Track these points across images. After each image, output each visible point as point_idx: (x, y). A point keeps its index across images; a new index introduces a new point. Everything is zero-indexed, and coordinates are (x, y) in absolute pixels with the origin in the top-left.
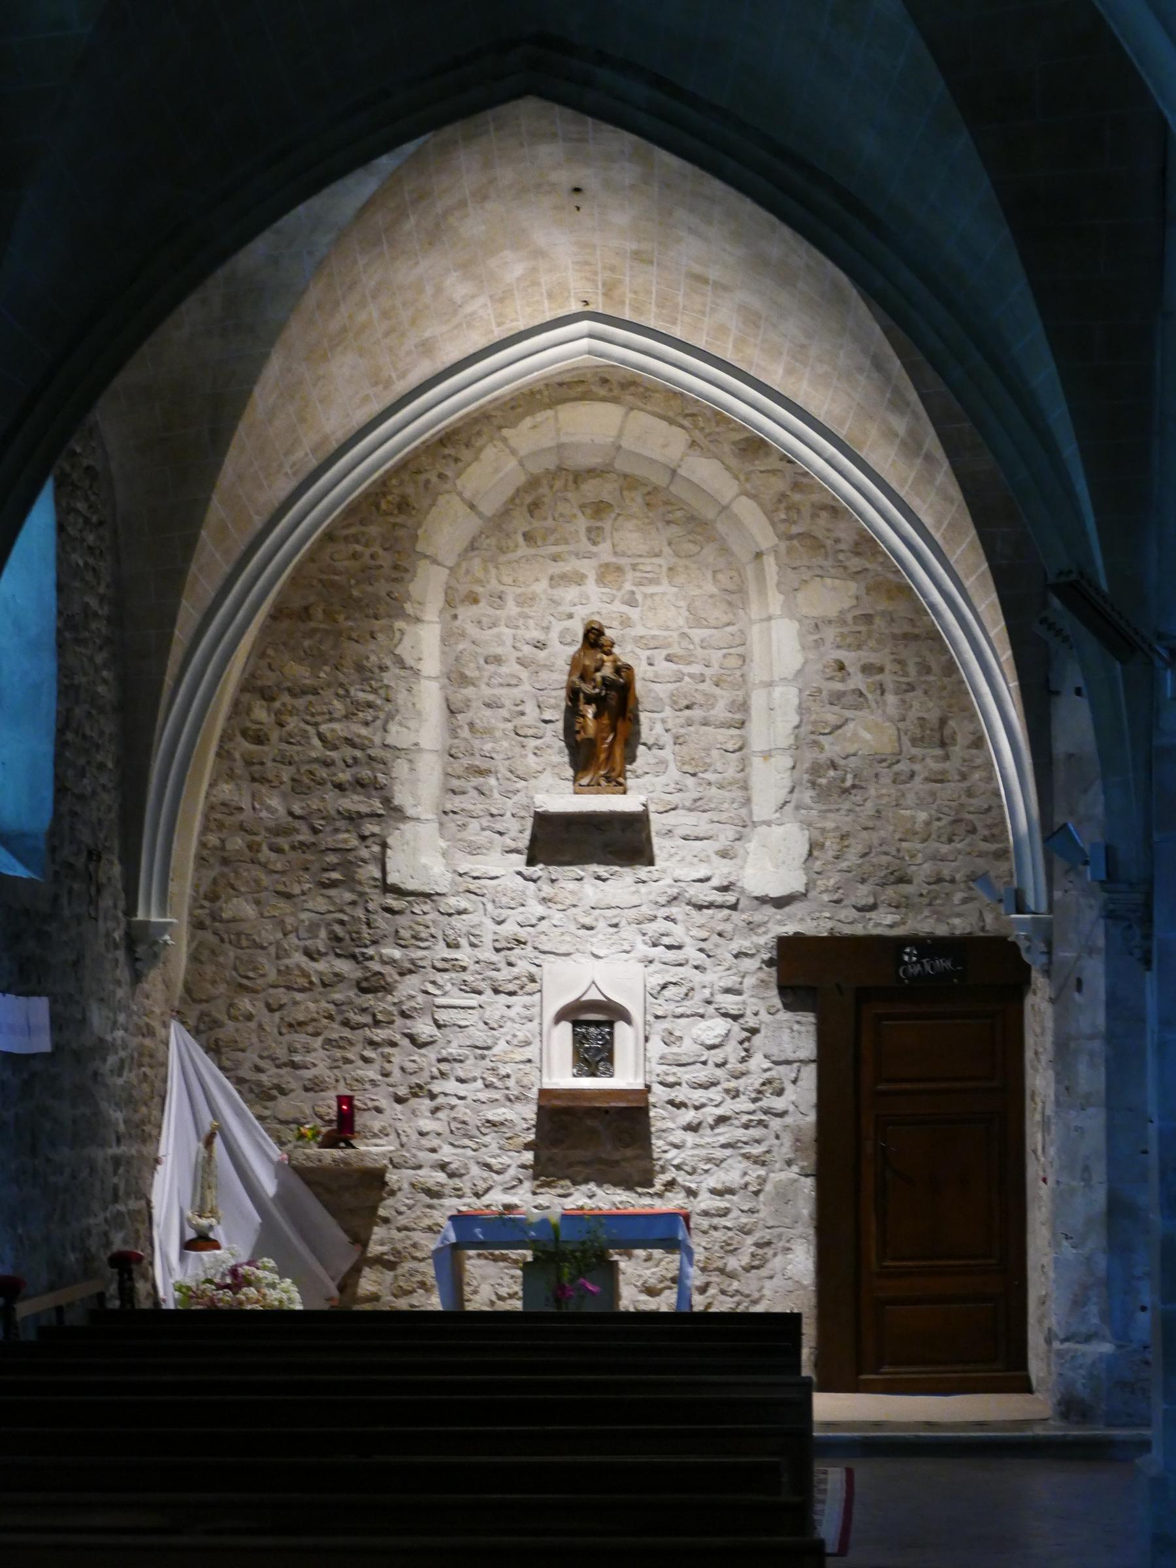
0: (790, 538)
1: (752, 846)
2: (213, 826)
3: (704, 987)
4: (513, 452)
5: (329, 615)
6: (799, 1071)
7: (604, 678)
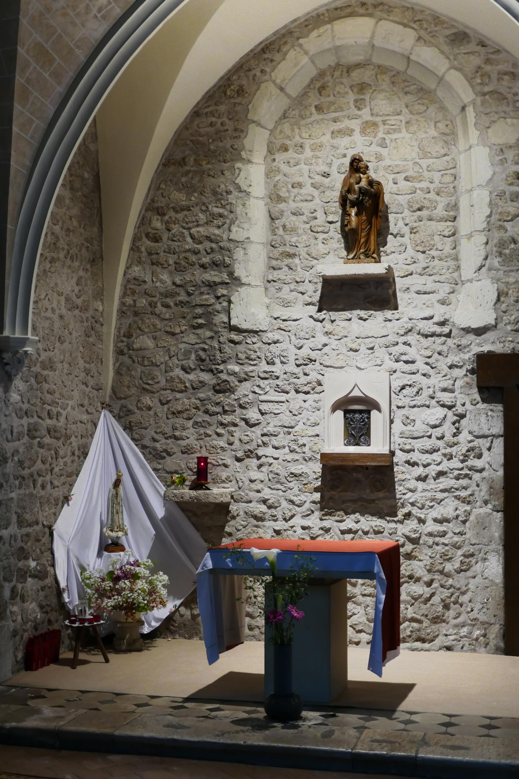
0: (484, 94)
1: (461, 297)
2: (129, 292)
3: (429, 387)
4: (306, 53)
5: (197, 162)
6: (492, 442)
7: (360, 188)
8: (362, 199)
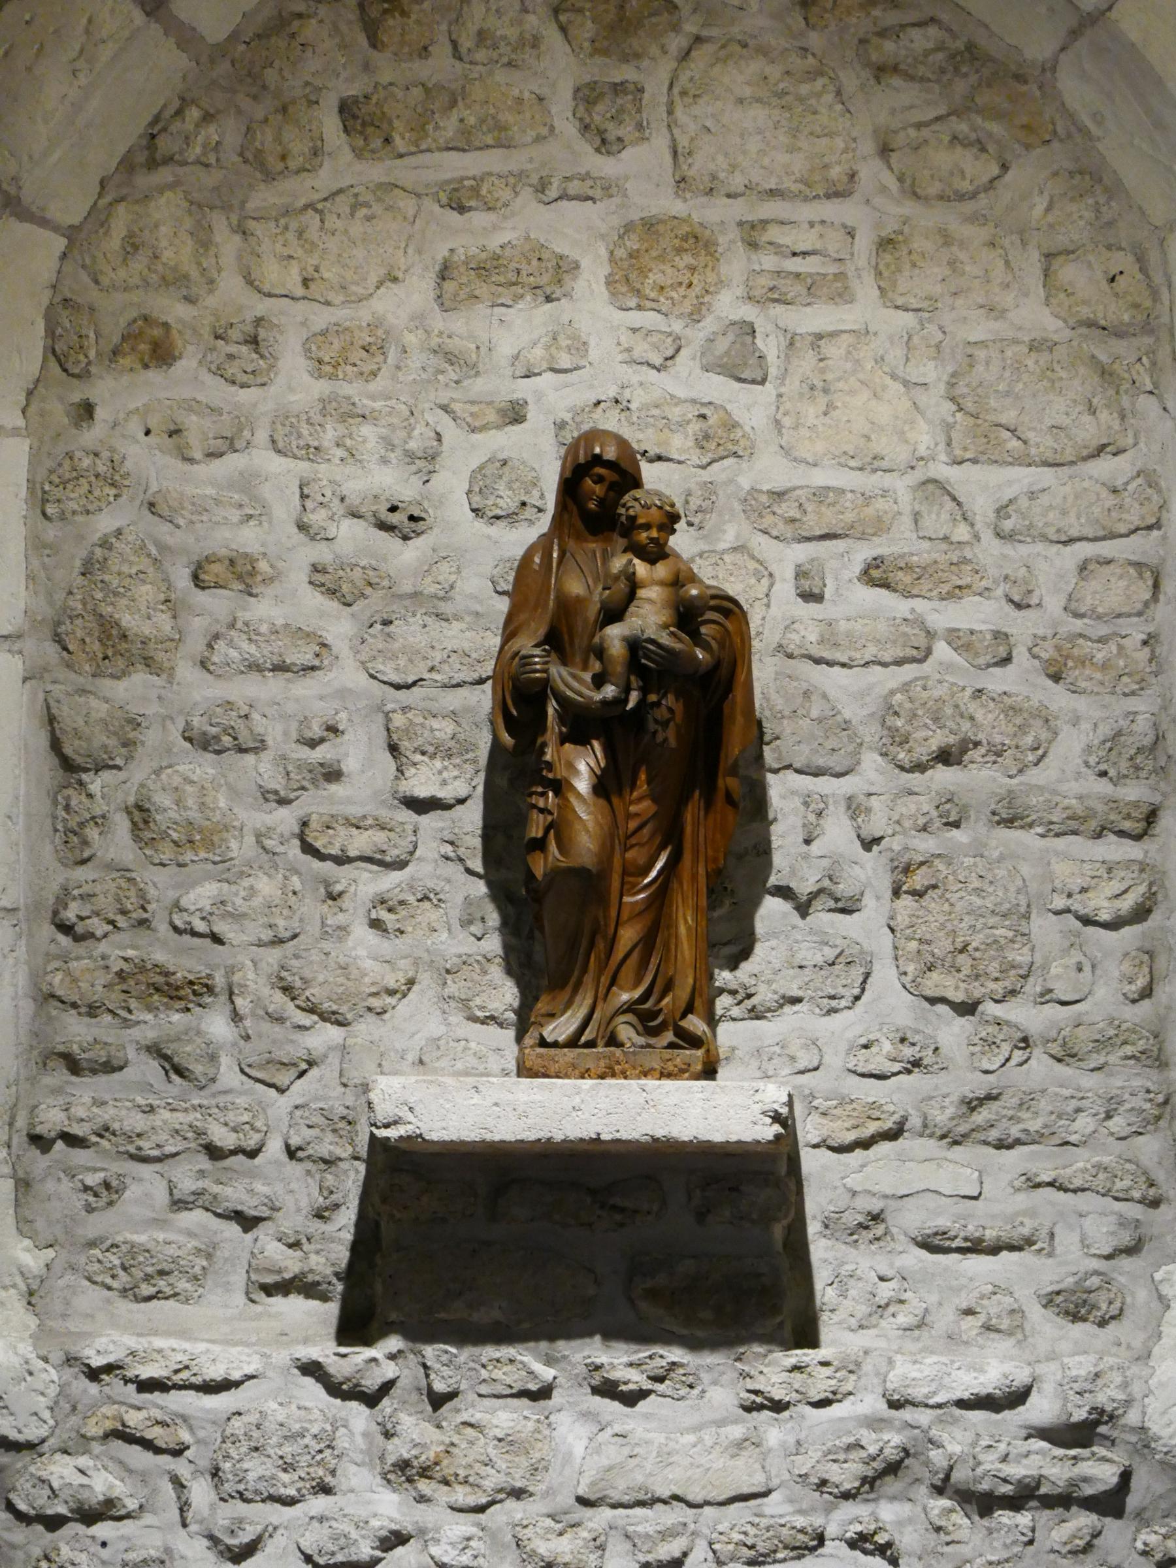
7: (634, 646)
8: (642, 703)
